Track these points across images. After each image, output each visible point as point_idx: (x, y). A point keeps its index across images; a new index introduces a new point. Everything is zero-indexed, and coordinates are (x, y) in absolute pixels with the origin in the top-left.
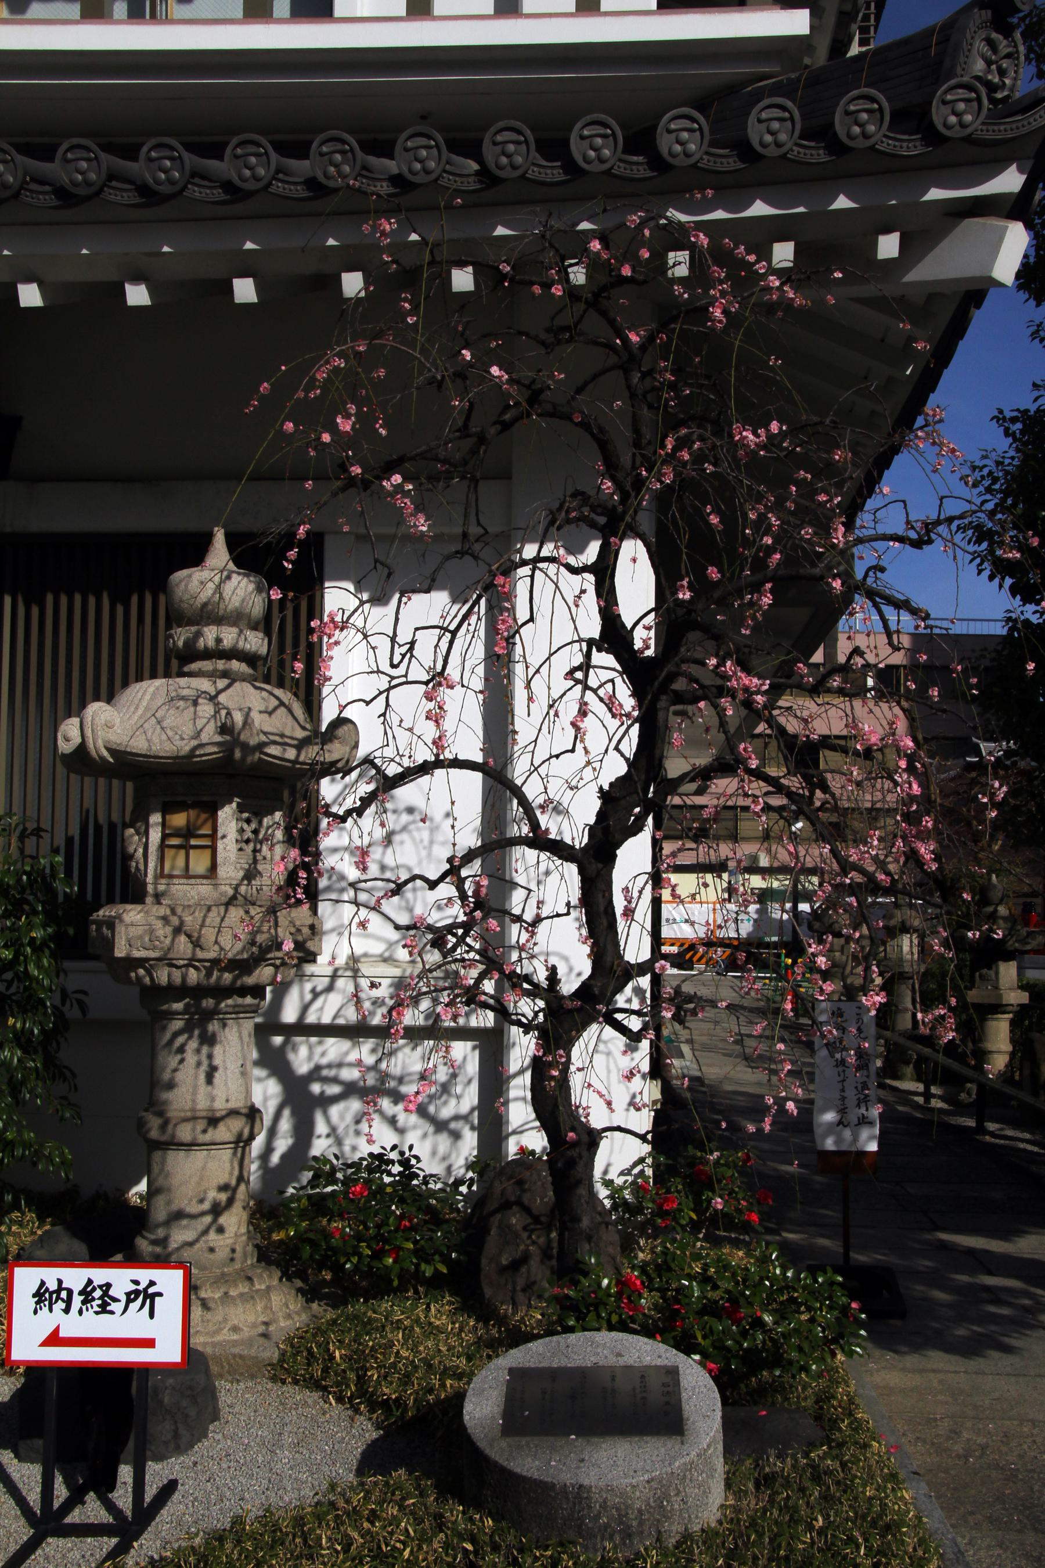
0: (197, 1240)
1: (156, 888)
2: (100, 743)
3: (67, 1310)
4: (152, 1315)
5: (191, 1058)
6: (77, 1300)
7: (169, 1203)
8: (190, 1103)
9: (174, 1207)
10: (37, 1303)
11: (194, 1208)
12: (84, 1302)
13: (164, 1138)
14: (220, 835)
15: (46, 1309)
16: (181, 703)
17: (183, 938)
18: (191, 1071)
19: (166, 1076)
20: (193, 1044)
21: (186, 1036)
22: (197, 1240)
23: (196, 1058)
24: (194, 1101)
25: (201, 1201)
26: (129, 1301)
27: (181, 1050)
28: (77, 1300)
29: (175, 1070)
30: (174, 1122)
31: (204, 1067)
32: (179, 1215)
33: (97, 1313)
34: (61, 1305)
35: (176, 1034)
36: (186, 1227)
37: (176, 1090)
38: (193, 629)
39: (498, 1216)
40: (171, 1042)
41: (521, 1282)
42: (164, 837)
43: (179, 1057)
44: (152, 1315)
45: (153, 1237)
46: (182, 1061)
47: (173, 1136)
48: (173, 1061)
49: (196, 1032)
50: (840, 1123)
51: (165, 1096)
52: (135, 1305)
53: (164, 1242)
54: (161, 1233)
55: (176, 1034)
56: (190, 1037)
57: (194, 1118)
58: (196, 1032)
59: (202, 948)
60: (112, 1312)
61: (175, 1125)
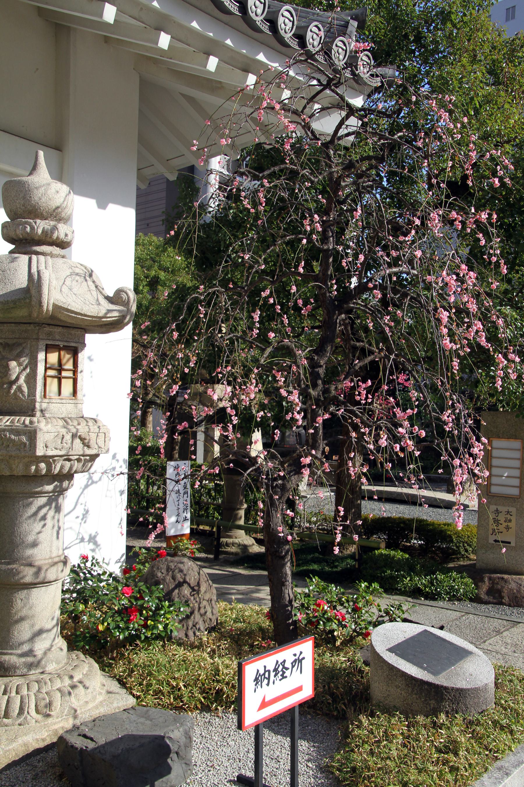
0: (52, 646)
1: (41, 406)
2: (51, 302)
3: (268, 684)
4: (301, 672)
5: (49, 522)
6: (272, 674)
7: (33, 626)
8: (49, 553)
9: (37, 628)
10: (256, 685)
11: (49, 626)
12: (275, 676)
13: (38, 580)
14: (79, 370)
15: (259, 687)
16: (78, 278)
17: (77, 441)
18: (50, 531)
19: (30, 538)
20: (52, 513)
21: (48, 507)
22: (52, 646)
23: (52, 523)
24: (51, 551)
25: (53, 619)
26: (293, 667)
27: (44, 518)
28: (272, 674)
29: (39, 533)
30: (45, 568)
31: (56, 528)
32: (40, 632)
33: (280, 680)
34: (266, 681)
35: (40, 508)
36: (45, 639)
37: (40, 547)
38: (52, 223)
39: (176, 591)
40: (35, 514)
41: (191, 624)
42: (46, 369)
43: (42, 523)
44: (301, 672)
45: (19, 652)
46: (44, 525)
47: (45, 578)
48: (37, 526)
49: (54, 505)
50: (177, 521)
51: (29, 552)
52: (295, 669)
53: (30, 653)
54: (25, 648)
55: (40, 508)
56: (50, 509)
57: (56, 563)
58: (54, 505)
59: (89, 447)
60: (286, 677)
61: (47, 570)
